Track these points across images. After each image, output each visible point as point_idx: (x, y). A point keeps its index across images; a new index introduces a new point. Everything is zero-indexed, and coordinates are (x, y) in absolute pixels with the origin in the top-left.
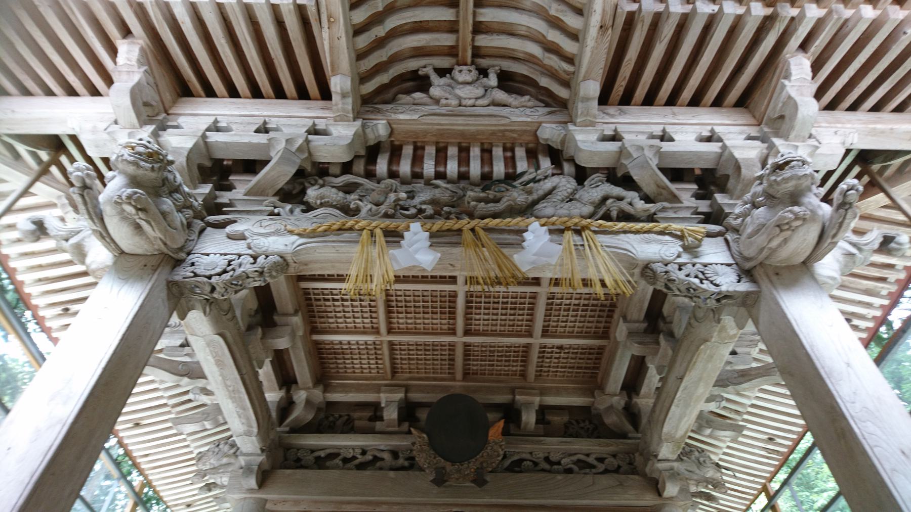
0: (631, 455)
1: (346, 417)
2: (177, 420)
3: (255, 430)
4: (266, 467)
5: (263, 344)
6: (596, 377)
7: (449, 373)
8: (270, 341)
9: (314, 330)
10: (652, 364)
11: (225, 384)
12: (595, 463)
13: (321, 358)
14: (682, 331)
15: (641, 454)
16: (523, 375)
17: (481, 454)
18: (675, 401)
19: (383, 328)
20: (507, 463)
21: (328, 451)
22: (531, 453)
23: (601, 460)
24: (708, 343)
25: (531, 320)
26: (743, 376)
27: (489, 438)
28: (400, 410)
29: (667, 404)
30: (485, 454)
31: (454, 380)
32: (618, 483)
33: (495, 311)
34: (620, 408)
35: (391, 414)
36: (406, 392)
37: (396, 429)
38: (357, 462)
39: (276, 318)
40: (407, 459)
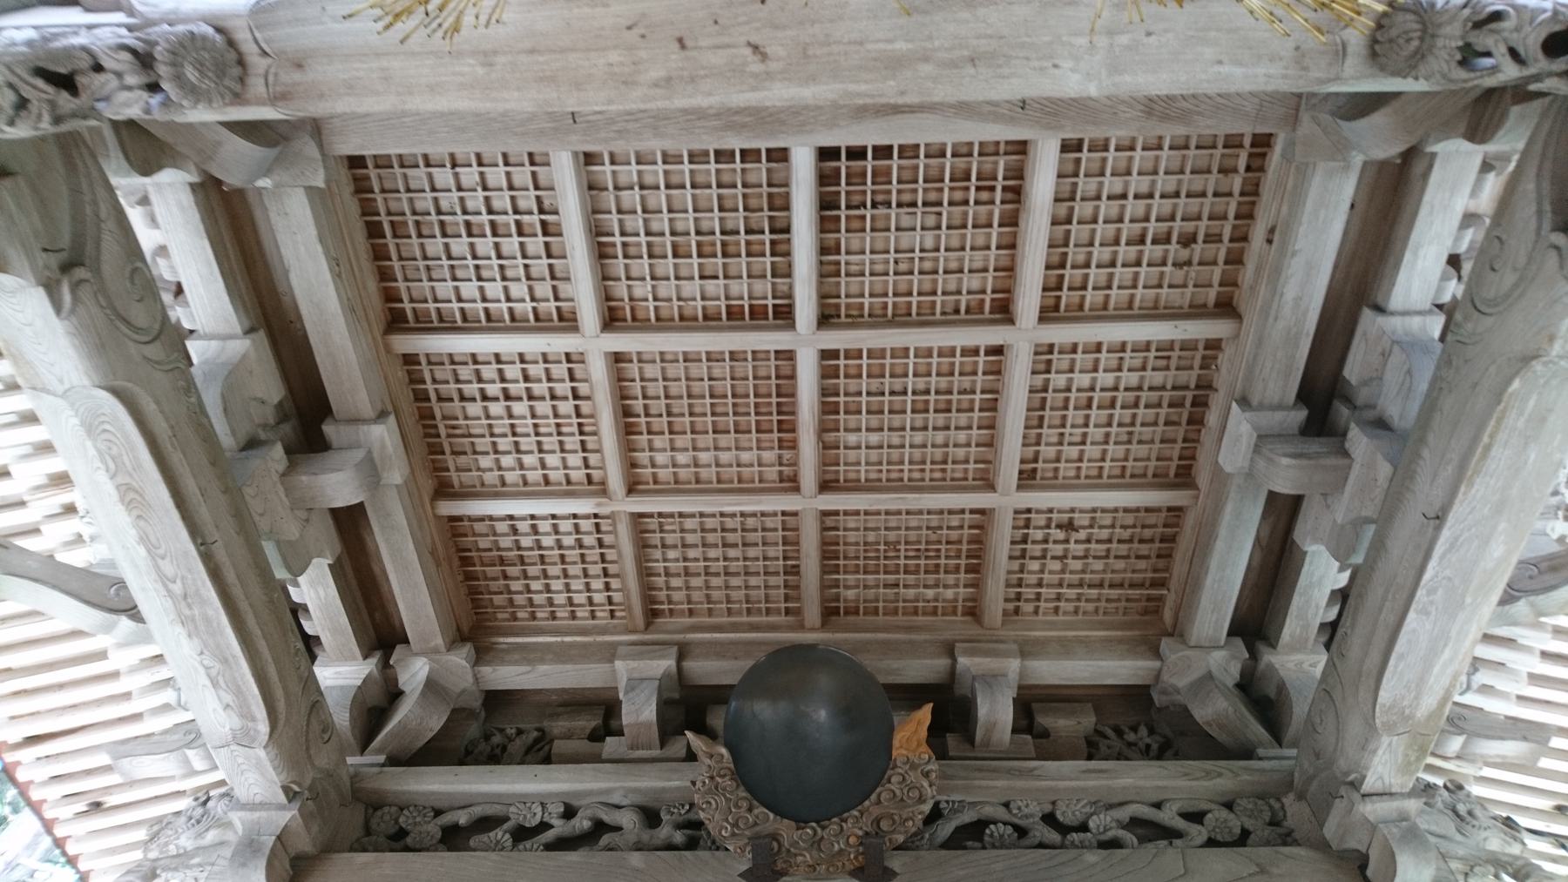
0: (1272, 801)
1: (535, 734)
2: (122, 748)
3: (263, 727)
4: (304, 843)
5: (288, 492)
6: (1157, 611)
7: (788, 611)
8: (304, 478)
9: (444, 490)
10: (1316, 540)
11: (157, 568)
12: (1180, 824)
13: (470, 577)
14: (1414, 408)
15: (1301, 797)
16: (974, 612)
17: (873, 797)
18: (1420, 593)
19: (615, 480)
20: (945, 829)
21: (478, 811)
22: (1006, 805)
23: (1196, 817)
24: (1537, 366)
25: (990, 444)
26: (1554, 569)
27: (894, 753)
28: (664, 705)
29: (1388, 617)
30: (884, 796)
31: (801, 627)
32: (1254, 869)
33: (897, 420)
34: (1230, 683)
35: (640, 711)
36: (681, 658)
37: (656, 753)
38: (549, 835)
39: (328, 429)
40: (679, 826)
